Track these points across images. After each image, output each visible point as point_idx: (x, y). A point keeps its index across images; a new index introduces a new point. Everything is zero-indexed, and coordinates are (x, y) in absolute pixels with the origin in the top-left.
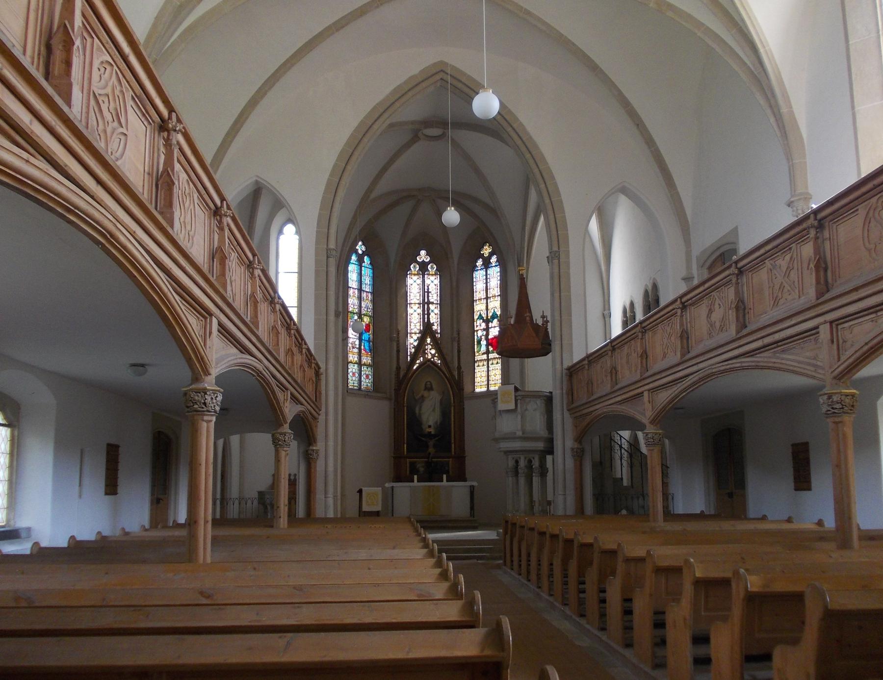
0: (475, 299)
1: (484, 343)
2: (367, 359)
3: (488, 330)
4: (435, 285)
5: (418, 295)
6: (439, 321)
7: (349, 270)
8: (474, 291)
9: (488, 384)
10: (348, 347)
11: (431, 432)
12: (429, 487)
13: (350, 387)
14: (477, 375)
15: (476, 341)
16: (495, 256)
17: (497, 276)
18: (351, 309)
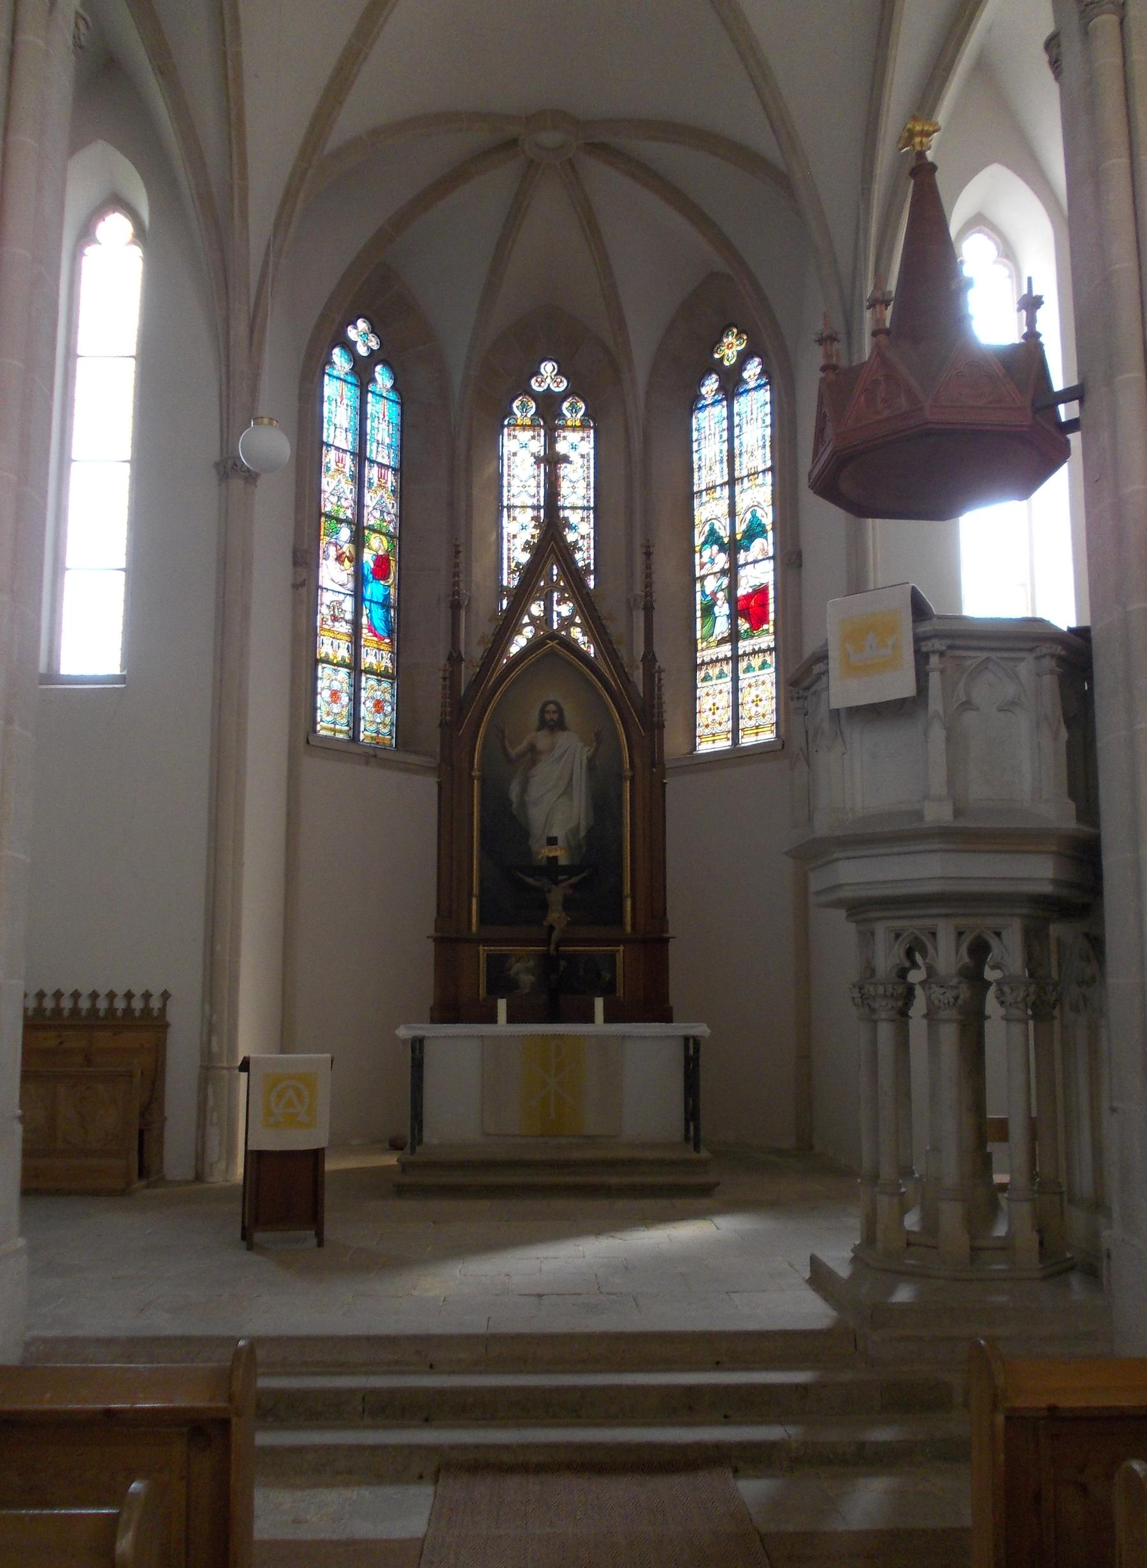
0: (696, 489)
1: (722, 609)
2: (376, 656)
3: (736, 574)
4: (582, 456)
5: (533, 483)
6: (592, 557)
7: (326, 394)
8: (695, 466)
9: (735, 730)
10: (319, 617)
11: (555, 858)
12: (544, 1037)
13: (323, 733)
14: (704, 703)
15: (698, 607)
16: (757, 360)
17: (761, 415)
18: (327, 508)
